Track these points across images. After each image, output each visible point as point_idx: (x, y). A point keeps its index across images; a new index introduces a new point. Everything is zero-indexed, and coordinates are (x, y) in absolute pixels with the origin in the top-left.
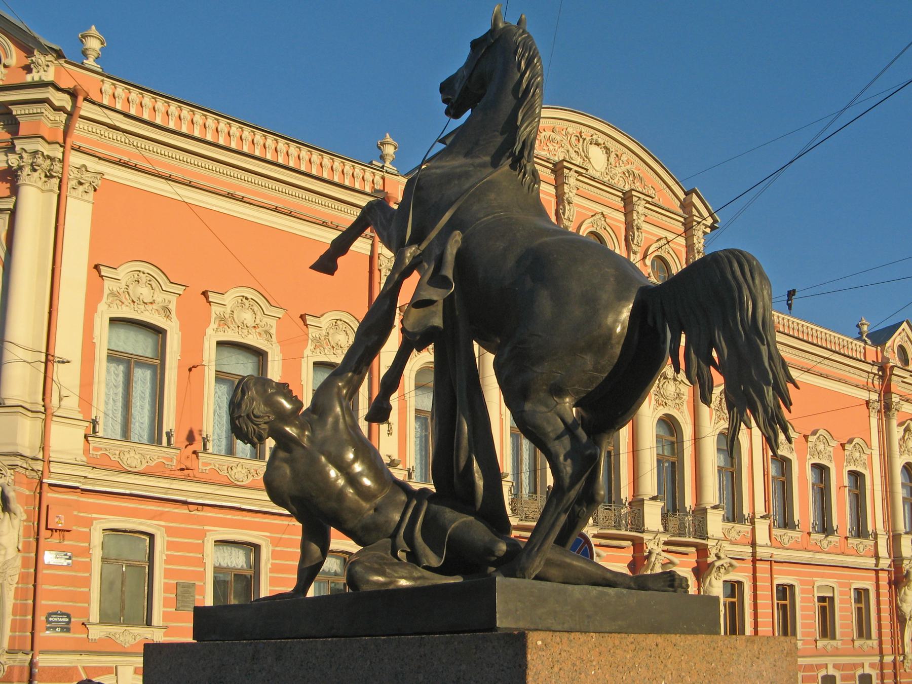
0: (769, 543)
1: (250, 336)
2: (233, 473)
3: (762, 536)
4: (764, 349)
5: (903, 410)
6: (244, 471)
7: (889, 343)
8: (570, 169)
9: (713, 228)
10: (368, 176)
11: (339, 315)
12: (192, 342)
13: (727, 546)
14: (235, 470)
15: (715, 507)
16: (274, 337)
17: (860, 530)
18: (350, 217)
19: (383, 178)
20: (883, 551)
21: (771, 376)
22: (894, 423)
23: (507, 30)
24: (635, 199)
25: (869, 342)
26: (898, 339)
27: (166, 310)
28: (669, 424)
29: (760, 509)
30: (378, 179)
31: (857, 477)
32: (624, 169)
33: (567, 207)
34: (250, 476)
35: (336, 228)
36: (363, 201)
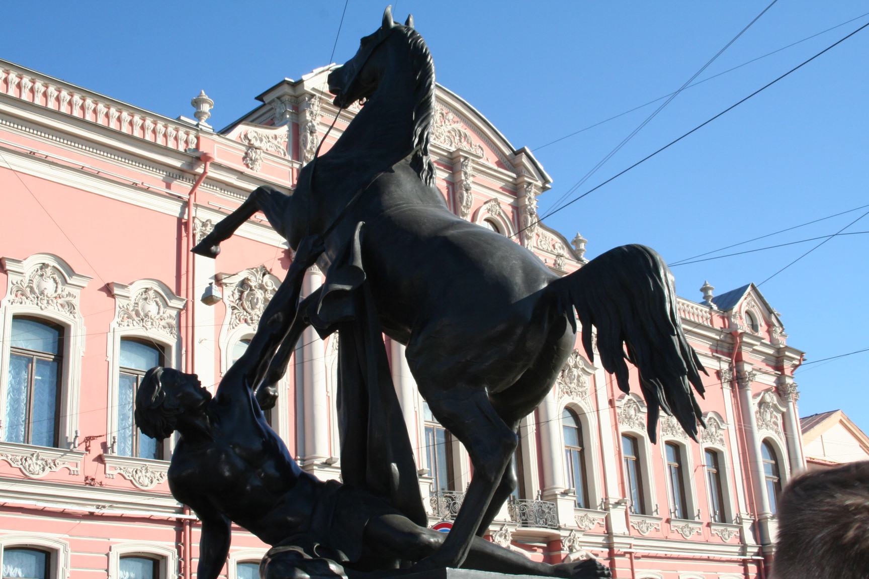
0: (627, 532)
1: (50, 307)
2: (27, 464)
3: (618, 525)
4: (675, 339)
5: (757, 380)
6: (39, 462)
7: (736, 308)
8: (466, 158)
9: (544, 189)
10: (182, 134)
11: (149, 284)
12: (96, 335)
13: (580, 537)
14: (29, 461)
15: (565, 493)
16: (77, 309)
17: (723, 516)
18: (234, 203)
19: (198, 138)
20: (749, 538)
21: (685, 365)
22: (750, 394)
23: (397, 30)
24: (462, 160)
25: (715, 307)
26: (745, 304)
27: (71, 307)
28: (574, 412)
29: (615, 495)
30: (192, 137)
31: (715, 455)
32: (449, 128)
33: (309, 137)
34: (47, 468)
35: (222, 213)
36: (253, 187)
